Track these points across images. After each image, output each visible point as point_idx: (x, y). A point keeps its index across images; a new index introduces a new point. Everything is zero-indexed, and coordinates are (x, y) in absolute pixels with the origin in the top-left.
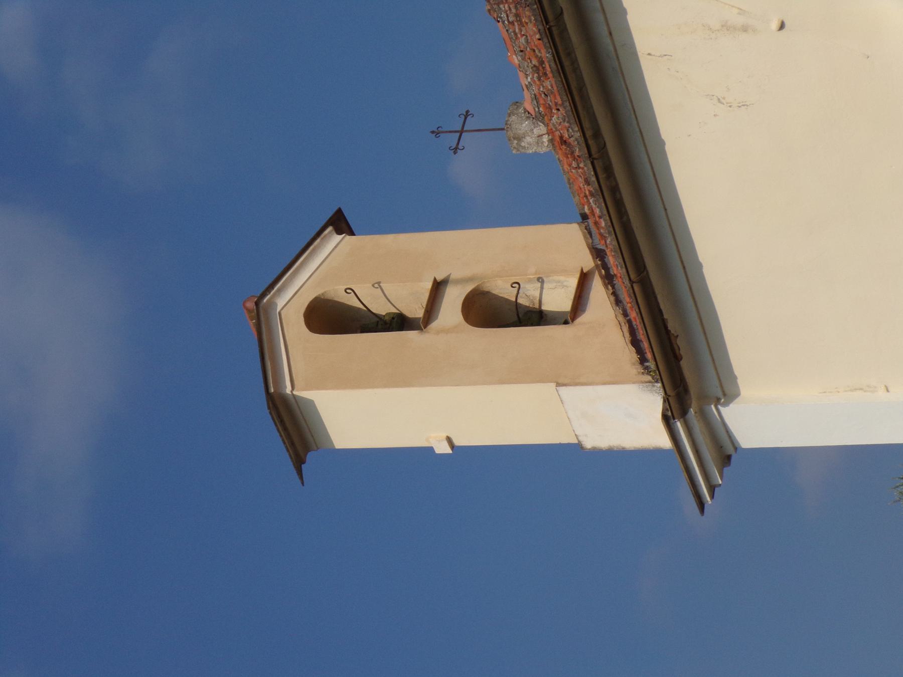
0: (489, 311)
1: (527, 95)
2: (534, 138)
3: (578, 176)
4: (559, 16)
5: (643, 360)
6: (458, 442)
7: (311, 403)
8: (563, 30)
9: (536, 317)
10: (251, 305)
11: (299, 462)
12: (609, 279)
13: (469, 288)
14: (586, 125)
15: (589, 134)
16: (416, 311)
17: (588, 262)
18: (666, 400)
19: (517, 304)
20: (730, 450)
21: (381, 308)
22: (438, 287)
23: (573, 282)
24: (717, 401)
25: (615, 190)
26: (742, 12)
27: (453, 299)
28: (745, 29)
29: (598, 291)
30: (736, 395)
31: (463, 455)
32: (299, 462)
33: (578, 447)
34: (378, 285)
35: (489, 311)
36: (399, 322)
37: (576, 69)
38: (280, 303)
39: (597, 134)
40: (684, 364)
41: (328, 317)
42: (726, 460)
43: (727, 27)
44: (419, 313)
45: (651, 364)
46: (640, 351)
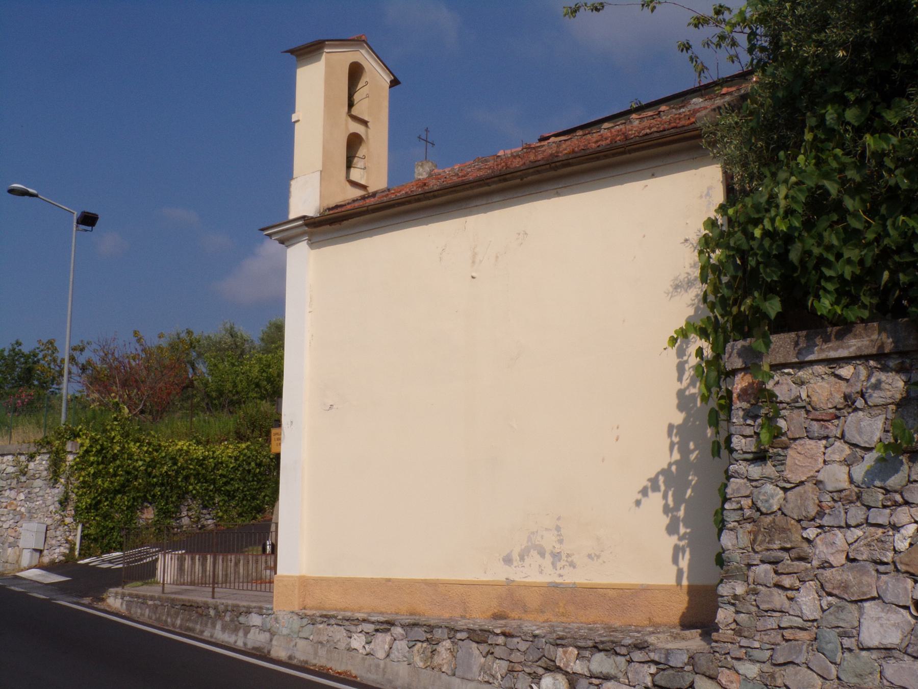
0: (354, 143)
1: (441, 171)
2: (422, 172)
3: (407, 187)
4: (488, 185)
5: (329, 209)
6: (297, 125)
7: (319, 60)
8: (481, 186)
9: (349, 165)
10: (363, 38)
11: (292, 52)
12: (363, 198)
13: (364, 137)
14: (440, 192)
15: (436, 193)
16: (355, 111)
17: (371, 189)
18: (312, 218)
19: (355, 157)
20: (287, 244)
21: (357, 97)
22: (365, 123)
23: (363, 182)
24: (309, 240)
25: (409, 202)
26: (481, 261)
27: (359, 129)
28: (474, 262)
29: (359, 193)
30: (312, 249)
31: (290, 128)
32: (292, 52)
33: (291, 177)
34: (367, 96)
35: (354, 143)
36: (351, 105)
37: (464, 190)
38: (363, 51)
39: (435, 197)
40: (328, 226)
41: (355, 72)
42: (282, 242)
43: (475, 255)
44: (355, 111)
45: (327, 213)
46: (333, 208)
